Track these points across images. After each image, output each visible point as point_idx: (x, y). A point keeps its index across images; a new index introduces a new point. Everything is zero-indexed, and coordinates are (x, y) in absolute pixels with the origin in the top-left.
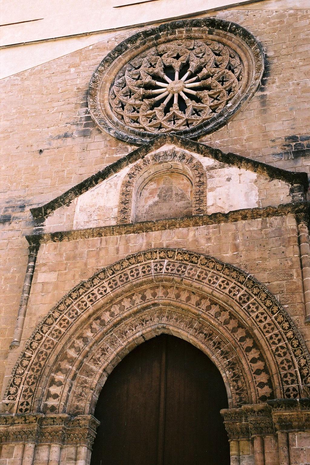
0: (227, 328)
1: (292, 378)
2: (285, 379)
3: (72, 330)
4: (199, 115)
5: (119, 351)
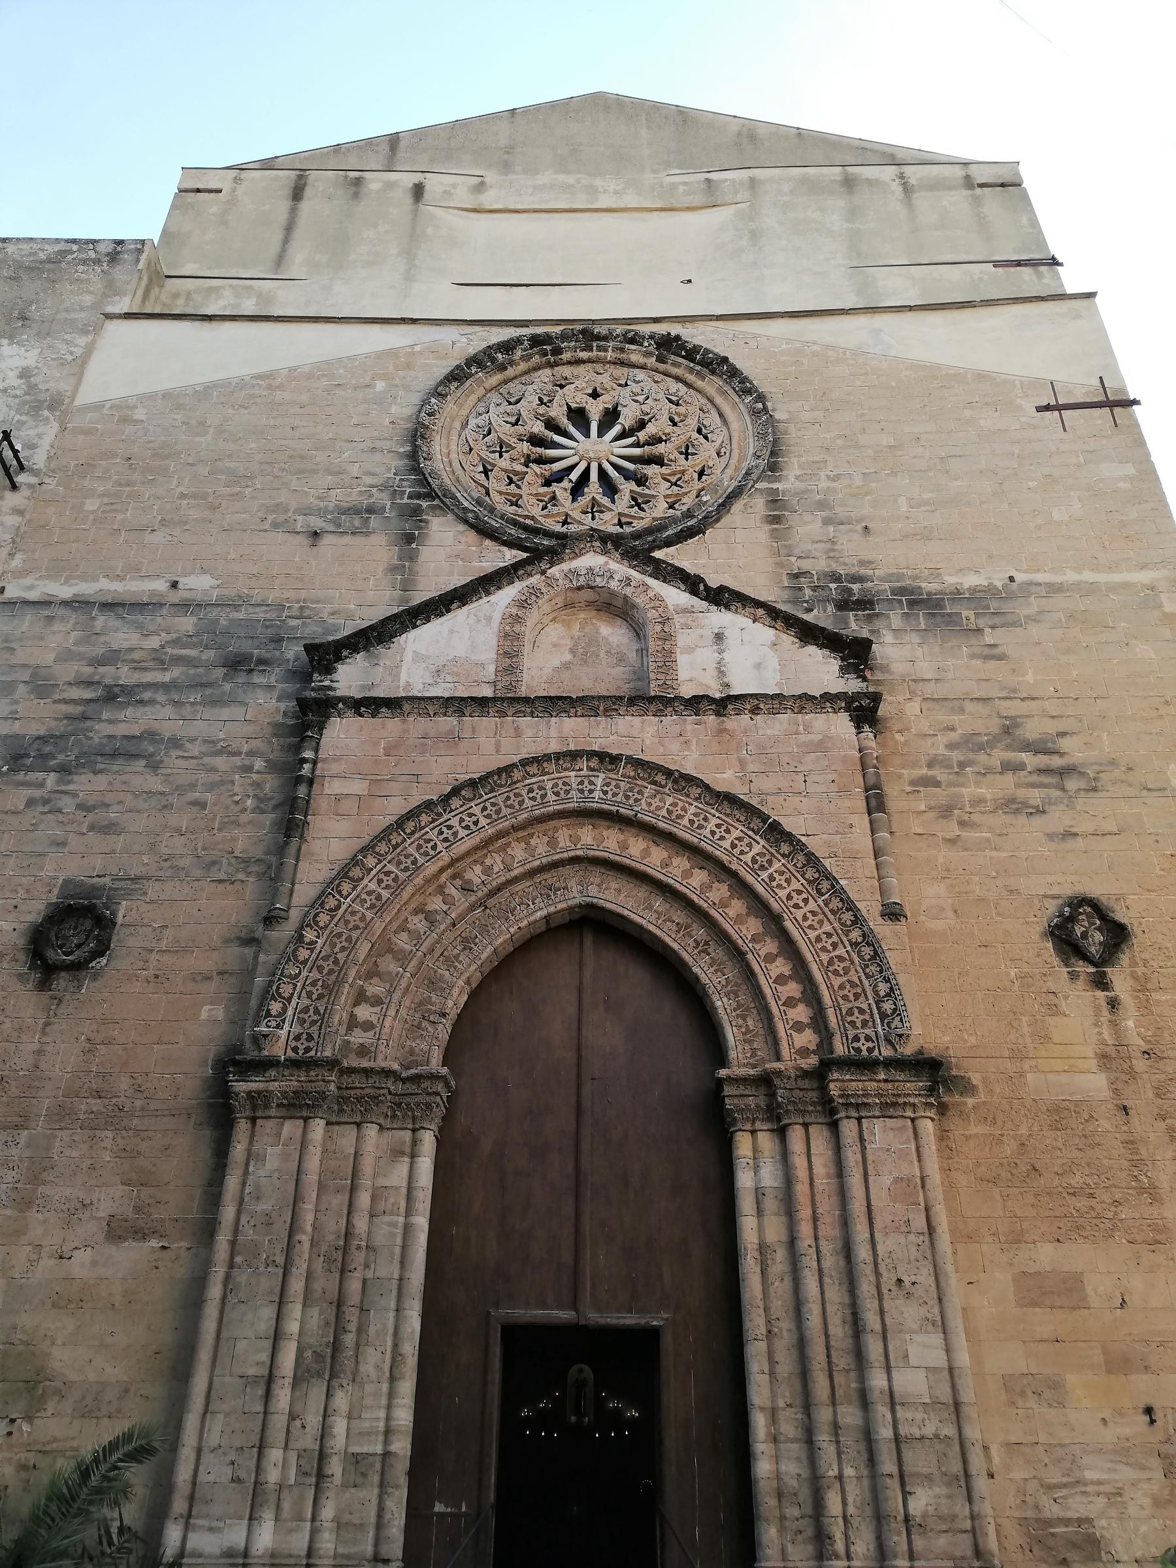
1: (862, 1017)
2: (849, 1019)
3: (405, 895)
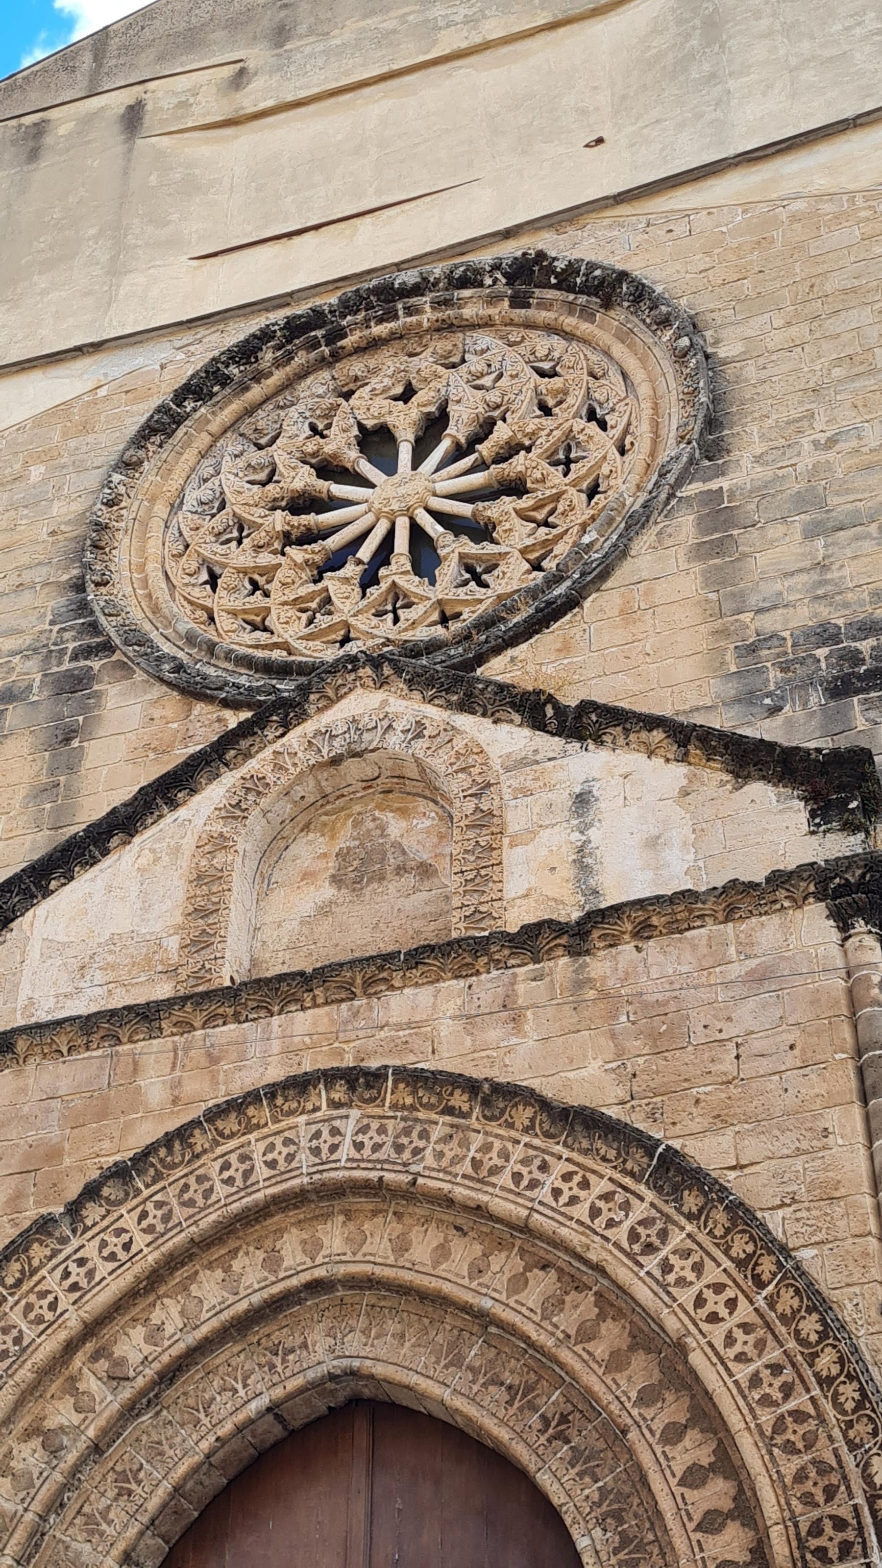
0: (589, 1353)
1: (840, 1536)
2: (814, 1543)
4: (486, 585)
5: (186, 1478)
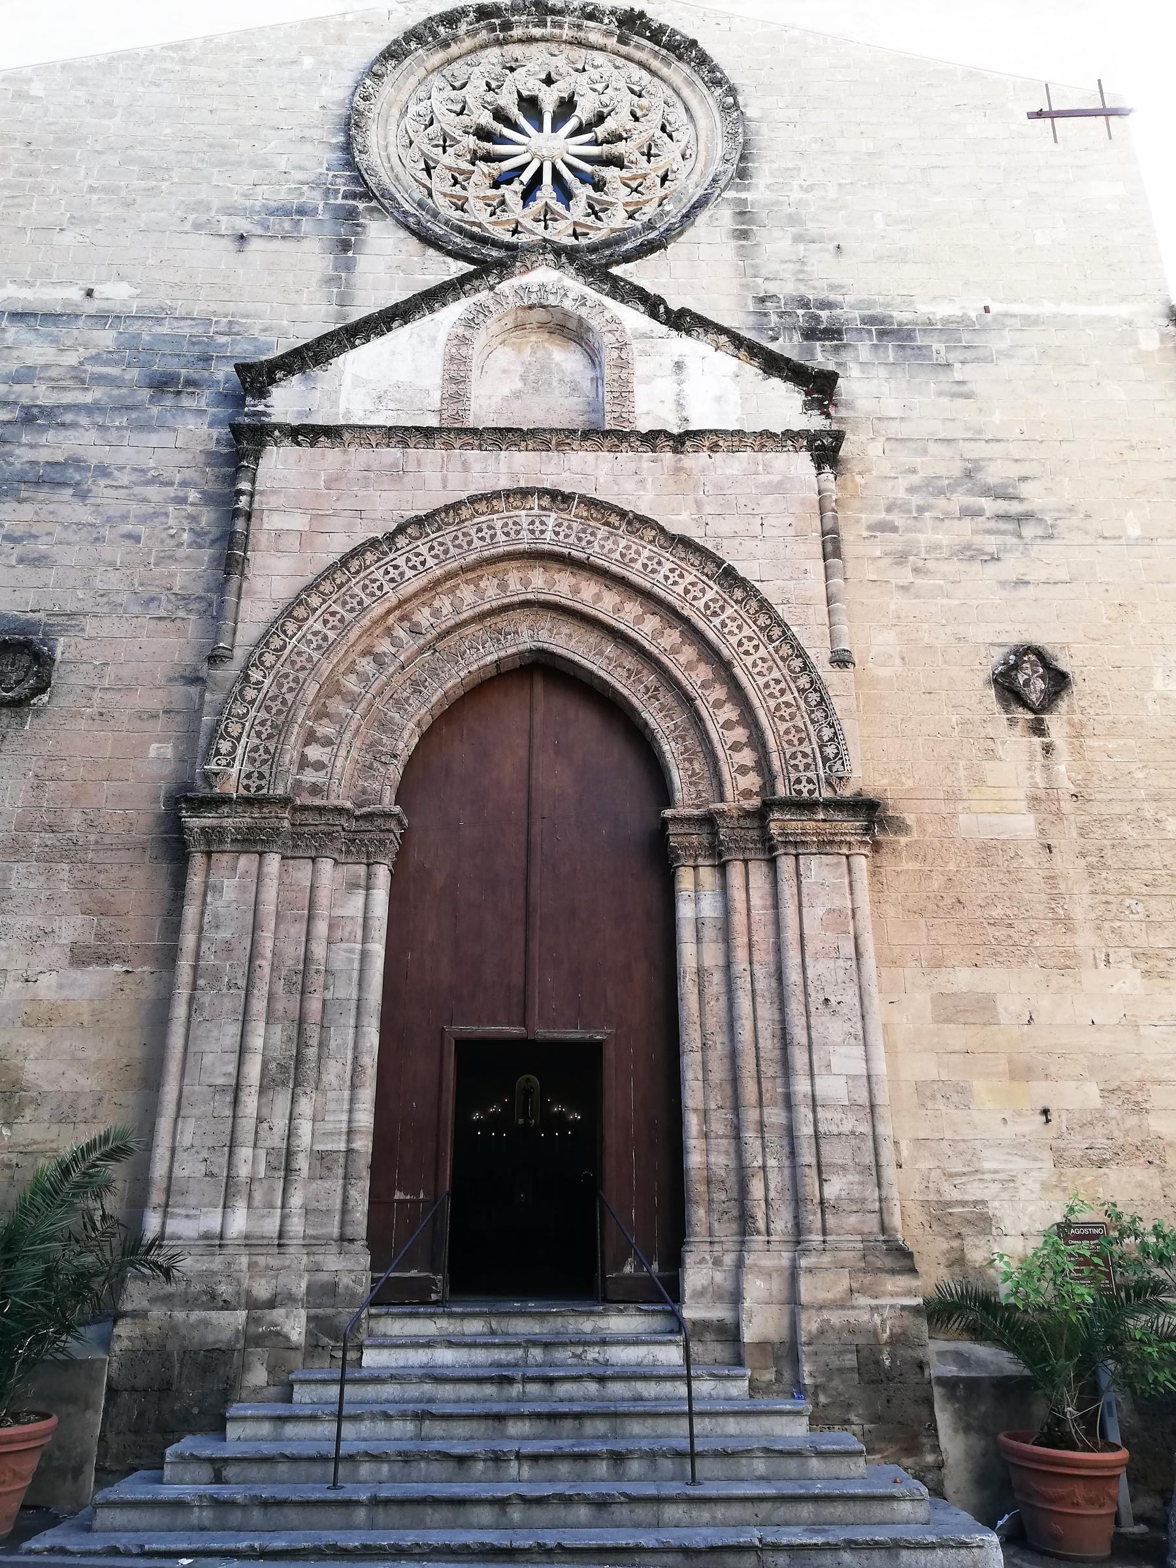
1: (805, 761)
2: (792, 762)
4: (600, 219)
